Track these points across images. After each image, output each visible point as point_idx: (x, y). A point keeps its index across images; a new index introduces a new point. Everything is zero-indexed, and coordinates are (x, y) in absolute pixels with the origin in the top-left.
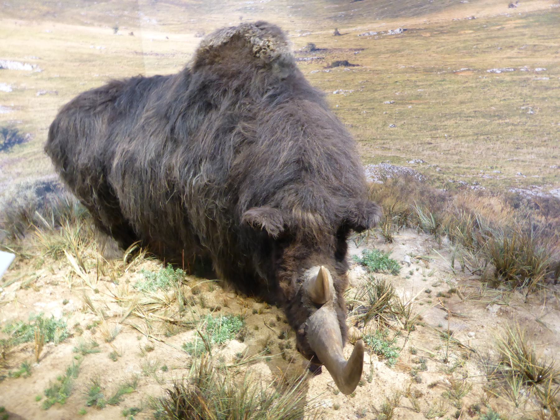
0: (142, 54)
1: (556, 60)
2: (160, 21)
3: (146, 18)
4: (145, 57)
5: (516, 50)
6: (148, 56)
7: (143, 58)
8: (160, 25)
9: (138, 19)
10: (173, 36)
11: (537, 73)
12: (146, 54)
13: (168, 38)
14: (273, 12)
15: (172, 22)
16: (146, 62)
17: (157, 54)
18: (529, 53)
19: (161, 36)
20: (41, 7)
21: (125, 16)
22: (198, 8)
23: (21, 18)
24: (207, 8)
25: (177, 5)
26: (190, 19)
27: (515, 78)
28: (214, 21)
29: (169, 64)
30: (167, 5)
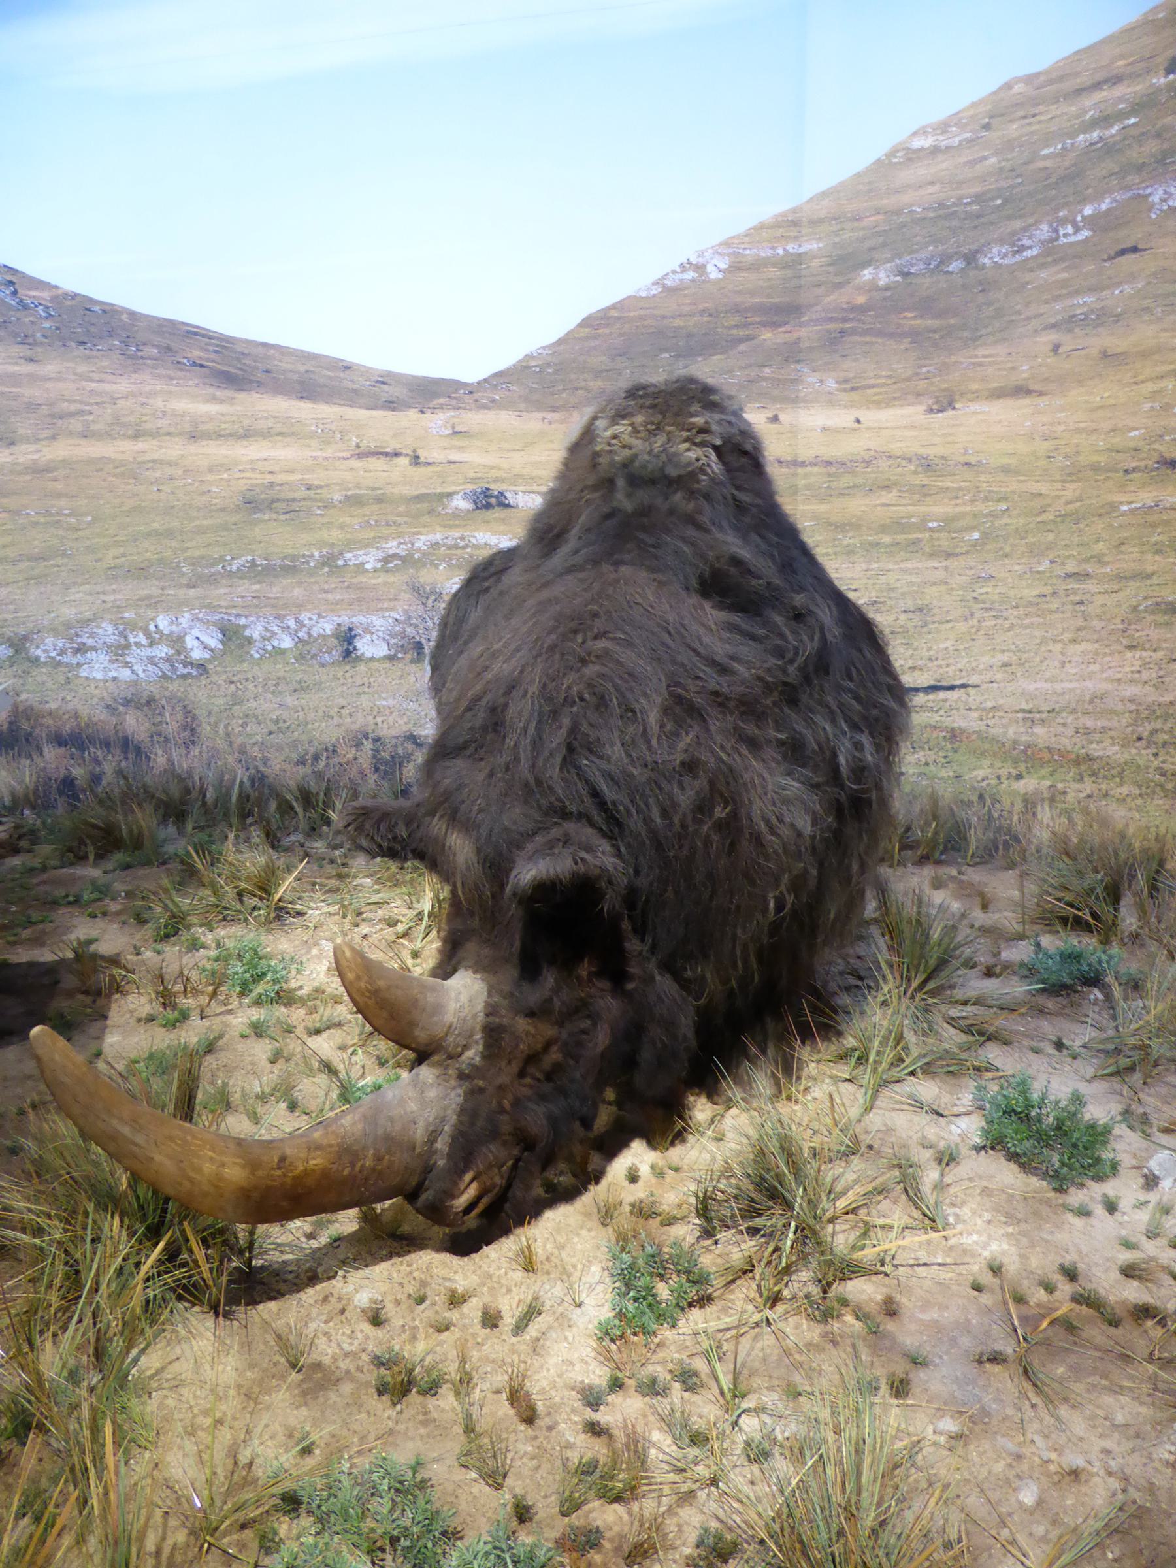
0: (795, 463)
1: (958, 510)
2: (846, 381)
3: (812, 379)
4: (800, 470)
5: (895, 493)
6: (809, 469)
7: (795, 475)
8: (845, 390)
9: (795, 381)
10: (871, 417)
11: (932, 530)
12: (803, 464)
13: (858, 421)
14: (1146, 318)
15: (872, 381)
16: (802, 483)
17: (829, 463)
18: (916, 497)
19: (842, 418)
20: (591, 384)
21: (765, 379)
22: (942, 337)
23: (554, 409)
24: (966, 334)
25: (891, 335)
26: (920, 367)
27: (900, 538)
28: (981, 364)
29: (854, 487)
30: (868, 339)
